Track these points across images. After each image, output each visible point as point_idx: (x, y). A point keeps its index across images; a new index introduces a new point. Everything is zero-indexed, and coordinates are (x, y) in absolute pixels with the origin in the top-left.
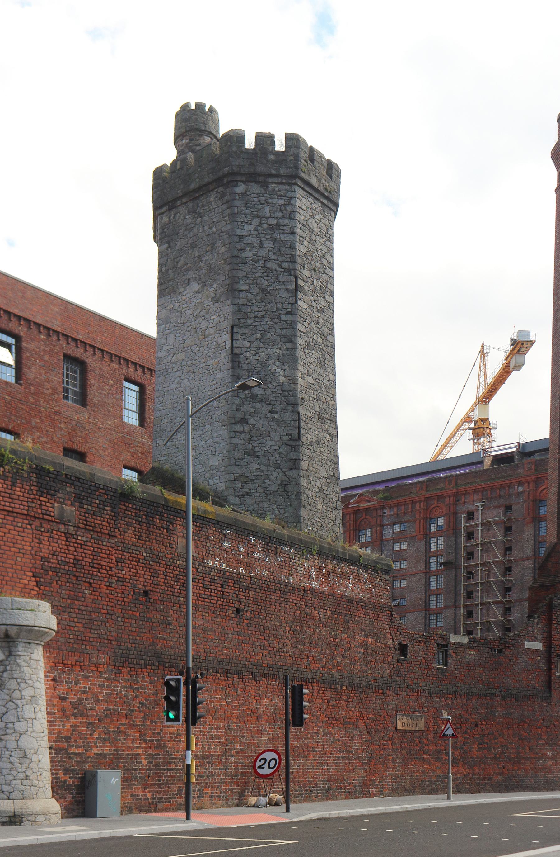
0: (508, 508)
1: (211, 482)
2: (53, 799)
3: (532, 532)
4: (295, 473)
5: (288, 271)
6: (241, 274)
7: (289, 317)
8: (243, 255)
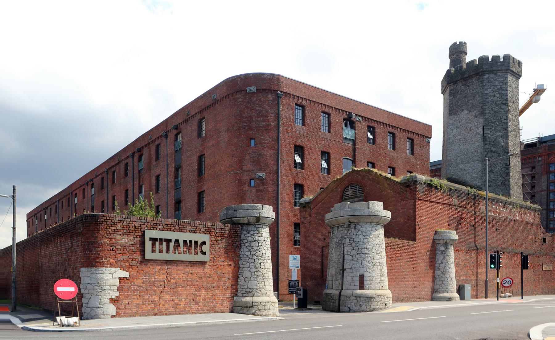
0: (533, 168)
1: (474, 182)
2: (111, 304)
3: (546, 179)
4: (508, 177)
5: (505, 104)
6: (487, 107)
7: (505, 121)
8: (487, 100)
